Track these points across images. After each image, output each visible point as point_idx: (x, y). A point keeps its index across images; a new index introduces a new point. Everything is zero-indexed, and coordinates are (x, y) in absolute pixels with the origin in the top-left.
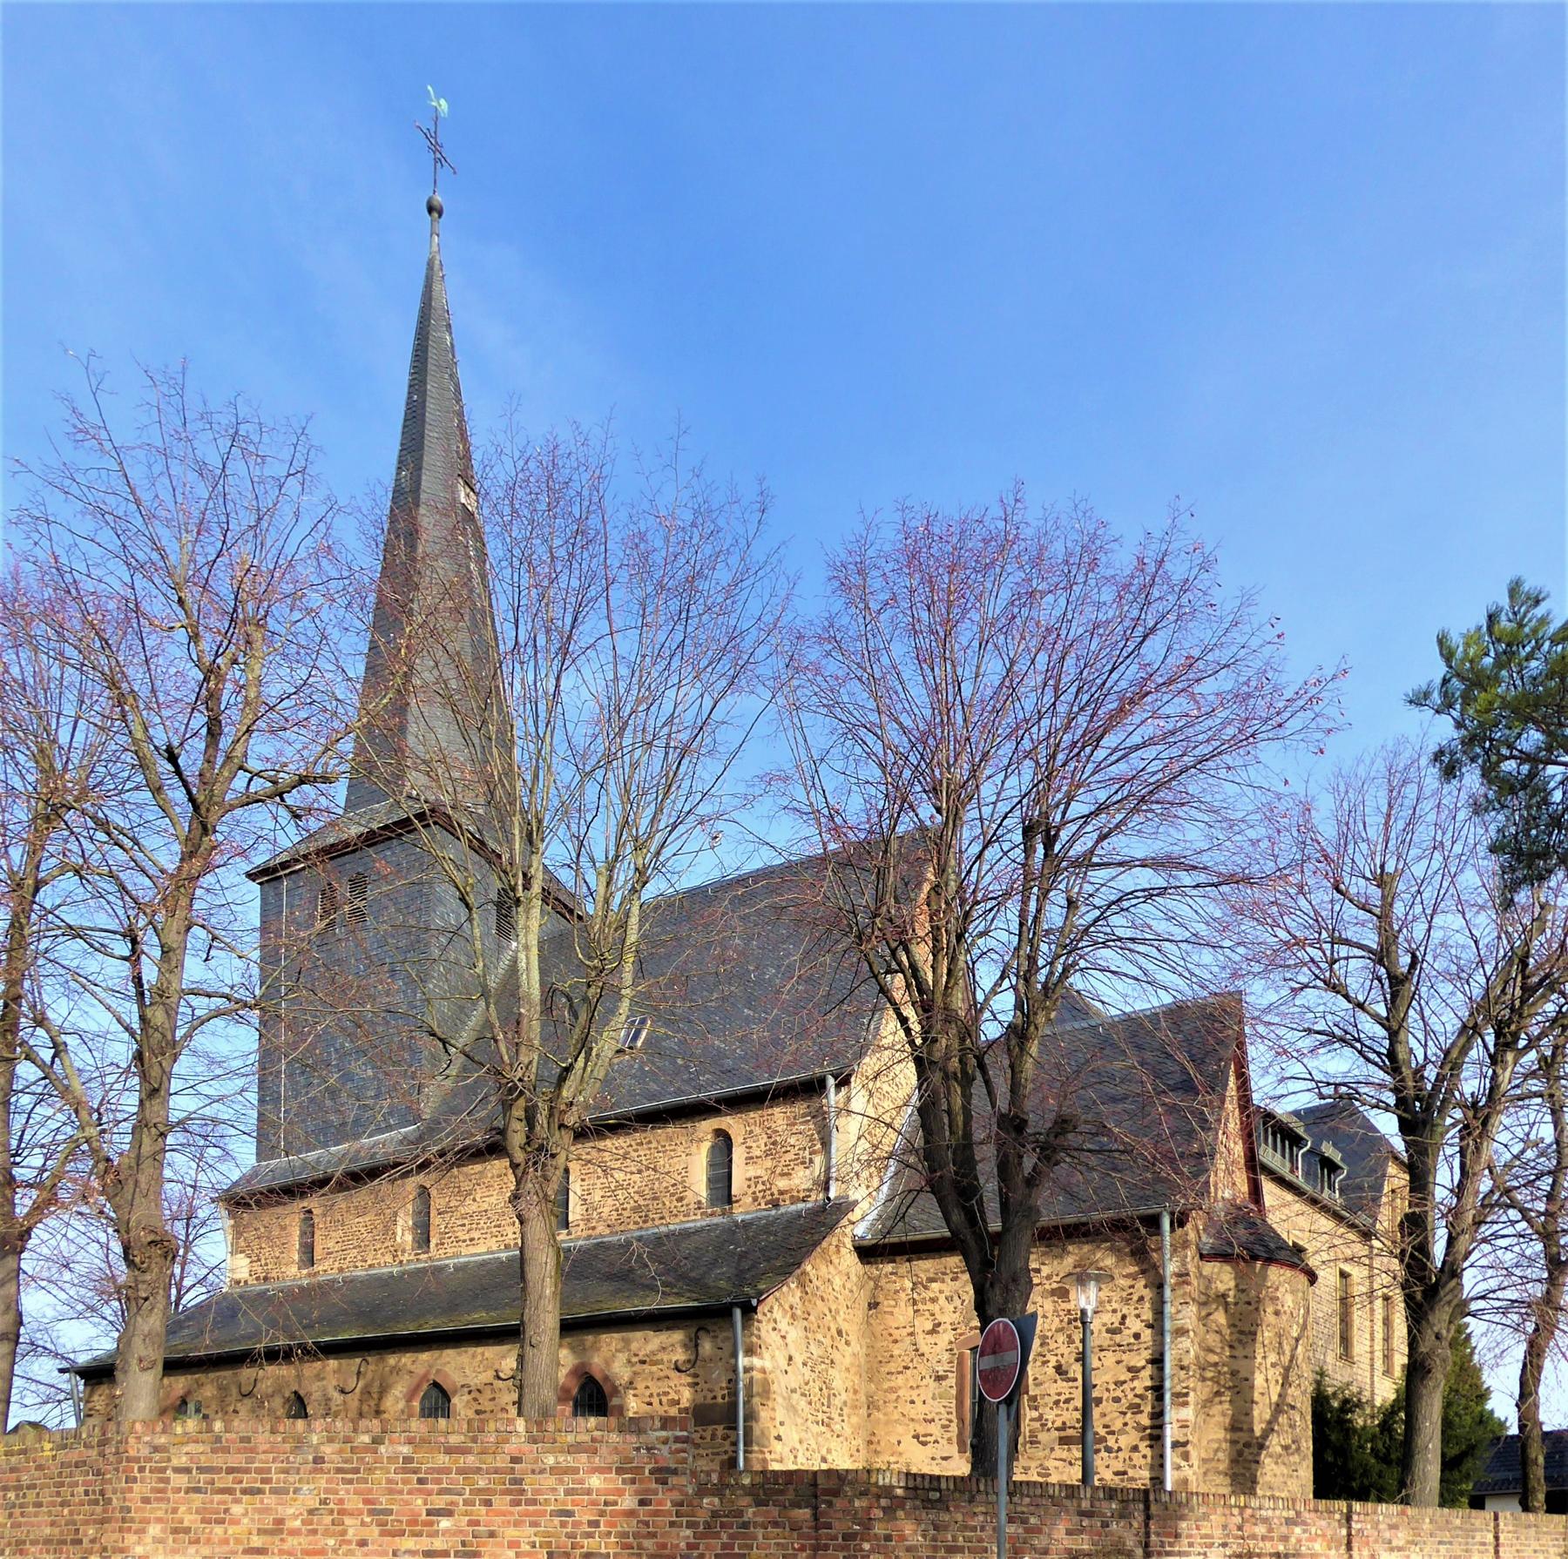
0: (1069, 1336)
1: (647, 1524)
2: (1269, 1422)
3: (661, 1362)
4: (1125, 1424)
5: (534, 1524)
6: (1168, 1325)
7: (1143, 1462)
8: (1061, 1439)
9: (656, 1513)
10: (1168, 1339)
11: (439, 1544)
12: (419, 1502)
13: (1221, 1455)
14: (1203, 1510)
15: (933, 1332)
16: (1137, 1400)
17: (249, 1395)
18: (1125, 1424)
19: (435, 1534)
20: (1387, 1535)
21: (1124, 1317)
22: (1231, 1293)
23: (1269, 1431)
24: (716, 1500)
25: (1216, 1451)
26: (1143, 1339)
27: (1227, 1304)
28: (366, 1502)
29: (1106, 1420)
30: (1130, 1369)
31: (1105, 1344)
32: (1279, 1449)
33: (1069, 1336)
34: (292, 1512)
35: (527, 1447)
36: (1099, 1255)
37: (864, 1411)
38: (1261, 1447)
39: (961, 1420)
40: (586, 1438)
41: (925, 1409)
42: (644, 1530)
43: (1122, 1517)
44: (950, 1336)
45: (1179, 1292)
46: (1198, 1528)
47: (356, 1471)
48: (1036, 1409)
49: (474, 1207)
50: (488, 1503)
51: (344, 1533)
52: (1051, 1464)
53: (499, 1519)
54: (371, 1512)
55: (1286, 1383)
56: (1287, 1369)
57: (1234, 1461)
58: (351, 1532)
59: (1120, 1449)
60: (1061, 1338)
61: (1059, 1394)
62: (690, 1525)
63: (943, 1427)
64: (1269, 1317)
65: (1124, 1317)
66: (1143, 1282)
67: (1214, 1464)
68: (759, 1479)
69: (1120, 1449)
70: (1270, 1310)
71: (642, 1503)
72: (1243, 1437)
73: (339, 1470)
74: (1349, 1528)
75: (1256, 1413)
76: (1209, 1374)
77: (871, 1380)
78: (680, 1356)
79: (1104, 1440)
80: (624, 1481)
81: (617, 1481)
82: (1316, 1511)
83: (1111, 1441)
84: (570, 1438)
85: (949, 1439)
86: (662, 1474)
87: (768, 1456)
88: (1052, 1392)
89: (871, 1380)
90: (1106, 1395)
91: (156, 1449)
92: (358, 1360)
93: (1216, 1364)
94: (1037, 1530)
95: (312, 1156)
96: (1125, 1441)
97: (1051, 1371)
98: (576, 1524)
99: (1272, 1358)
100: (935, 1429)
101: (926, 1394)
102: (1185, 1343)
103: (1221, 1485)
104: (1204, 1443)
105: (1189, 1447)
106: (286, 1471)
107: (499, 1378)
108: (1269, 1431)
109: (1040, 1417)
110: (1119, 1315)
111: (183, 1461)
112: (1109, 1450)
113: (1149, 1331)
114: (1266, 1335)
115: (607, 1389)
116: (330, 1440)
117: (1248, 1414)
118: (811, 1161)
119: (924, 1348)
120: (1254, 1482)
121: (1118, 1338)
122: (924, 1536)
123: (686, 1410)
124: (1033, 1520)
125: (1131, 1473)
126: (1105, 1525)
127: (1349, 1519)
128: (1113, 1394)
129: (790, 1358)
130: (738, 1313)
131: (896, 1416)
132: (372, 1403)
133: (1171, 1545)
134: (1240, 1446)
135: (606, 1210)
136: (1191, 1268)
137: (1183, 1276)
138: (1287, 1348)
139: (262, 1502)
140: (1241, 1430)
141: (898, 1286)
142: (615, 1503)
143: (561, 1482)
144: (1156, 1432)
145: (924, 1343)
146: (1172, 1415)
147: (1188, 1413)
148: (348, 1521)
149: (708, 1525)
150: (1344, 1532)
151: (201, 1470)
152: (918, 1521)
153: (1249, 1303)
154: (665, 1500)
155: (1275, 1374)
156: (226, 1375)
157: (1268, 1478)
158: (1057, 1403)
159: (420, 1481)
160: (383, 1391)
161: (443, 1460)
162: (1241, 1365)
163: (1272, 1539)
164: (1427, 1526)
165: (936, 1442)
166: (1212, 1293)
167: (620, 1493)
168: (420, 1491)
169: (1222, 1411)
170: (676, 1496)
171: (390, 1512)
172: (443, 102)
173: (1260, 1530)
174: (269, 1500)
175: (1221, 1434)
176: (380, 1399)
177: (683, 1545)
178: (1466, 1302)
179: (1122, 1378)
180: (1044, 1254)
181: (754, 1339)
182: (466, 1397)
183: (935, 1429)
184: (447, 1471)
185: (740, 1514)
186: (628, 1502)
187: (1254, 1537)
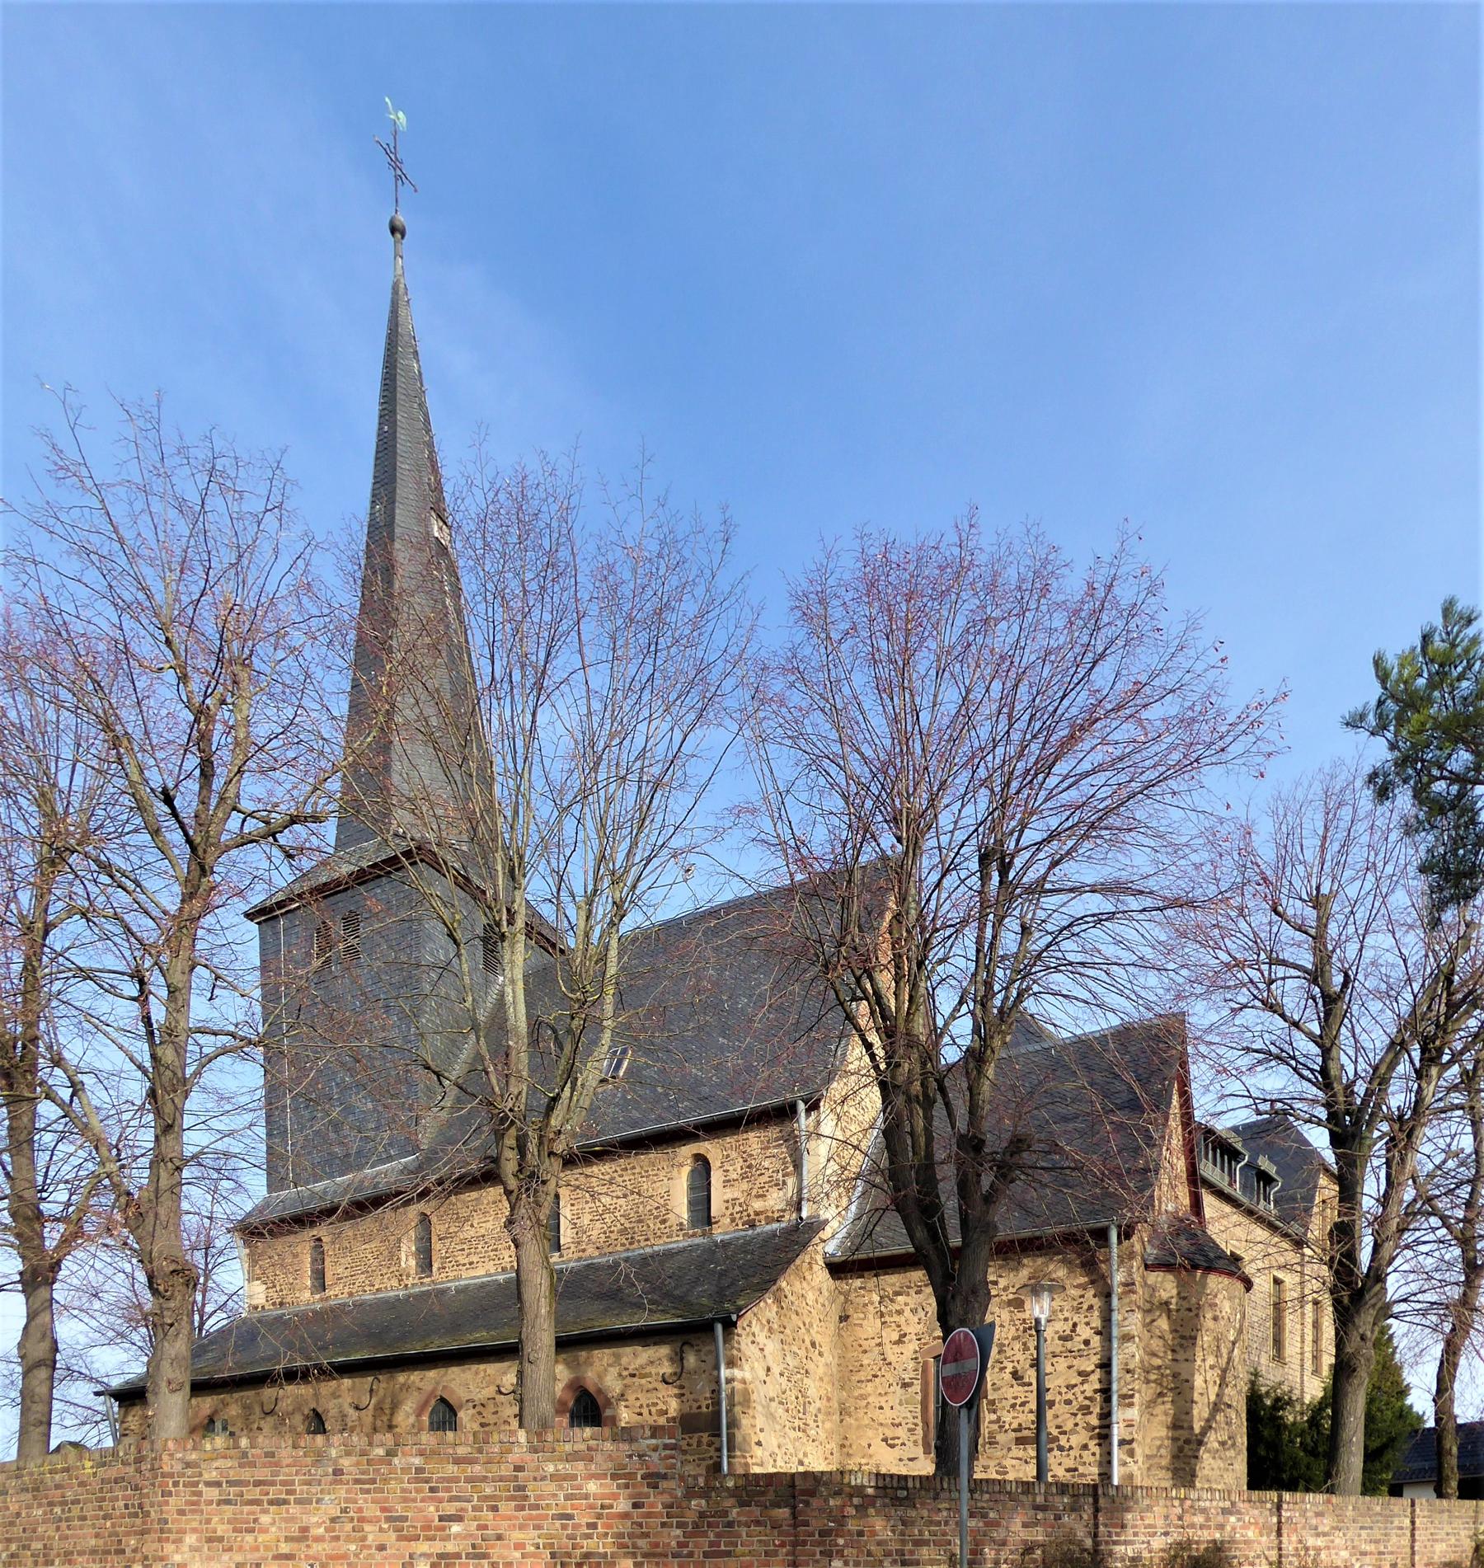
0: (1024, 1344)
1: (640, 1525)
2: (1208, 1420)
3: (649, 1375)
4: (1076, 1425)
5: (537, 1527)
6: (1115, 1332)
7: (1092, 1459)
8: (1017, 1439)
9: (649, 1515)
10: (1115, 1345)
11: (451, 1547)
12: (432, 1509)
13: (1163, 1451)
14: (1147, 1502)
15: (899, 1342)
16: (1087, 1402)
17: (271, 1413)
18: (1076, 1425)
19: (447, 1538)
20: (1314, 1522)
21: (1075, 1325)
22: (1174, 1301)
23: (1207, 1428)
24: (703, 1502)
25: (1159, 1448)
26: (1092, 1345)
27: (1169, 1311)
28: (383, 1510)
29: (1059, 1421)
30: (1080, 1374)
31: (1058, 1351)
32: (1216, 1445)
33: (1024, 1344)
34: (316, 1521)
35: (528, 1457)
36: (1051, 1267)
37: (836, 1417)
38: (1200, 1443)
39: (926, 1423)
40: (582, 1447)
41: (893, 1414)
42: (638, 1531)
43: (1073, 1510)
44: (914, 1346)
45: (1126, 1300)
46: (1142, 1519)
47: (373, 1481)
48: (994, 1412)
49: (472, 1233)
50: (495, 1509)
51: (364, 1539)
52: (1008, 1462)
53: (505, 1523)
54: (388, 1519)
55: (1223, 1383)
56: (1224, 1371)
57: (1175, 1457)
58: (370, 1537)
59: (1071, 1448)
60: (1017, 1346)
61: (1015, 1398)
62: (680, 1525)
63: (910, 1430)
64: (1209, 1323)
65: (1075, 1325)
66: (1092, 1292)
67: (1156, 1460)
68: (741, 1482)
69: (1071, 1448)
70: (1209, 1315)
71: (635, 1506)
72: (1184, 1434)
73: (357, 1481)
74: (1280, 1516)
75: (1195, 1412)
76: (1153, 1377)
77: (842, 1388)
78: (667, 1369)
79: (1056, 1439)
80: (618, 1487)
81: (612, 1486)
82: (1250, 1501)
83: (1063, 1441)
84: (568, 1447)
85: (915, 1442)
86: (654, 1479)
87: (749, 1460)
88: (1009, 1396)
89: (842, 1388)
90: (1058, 1398)
91: (188, 1465)
92: (370, 1379)
93: (1159, 1367)
94: (996, 1524)
95: (319, 1186)
96: (1076, 1441)
97: (1007, 1376)
98: (576, 1527)
99: (1211, 1360)
100: (901, 1432)
101: (893, 1400)
102: (1131, 1348)
103: (1163, 1479)
104: (1148, 1440)
105: (1135, 1445)
106: (308, 1483)
107: (501, 1393)
108: (1207, 1428)
109: (999, 1419)
110: (1071, 1323)
111: (213, 1475)
112: (1061, 1448)
113: (1098, 1338)
114: (1205, 1339)
115: (600, 1401)
116: (348, 1454)
117: (1188, 1413)
118: (784, 1183)
119: (891, 1358)
120: (1194, 1475)
121: (1069, 1344)
122: (893, 1531)
123: (674, 1419)
124: (992, 1515)
125: (1081, 1469)
126: (1058, 1518)
127: (1279, 1508)
128: (1065, 1397)
129: (768, 1369)
130: (719, 1327)
131: (866, 1421)
132: (385, 1419)
133: (1118, 1534)
134: (1180, 1443)
135: (595, 1233)
136: (1137, 1278)
137: (1129, 1285)
138: (1224, 1351)
139: (287, 1511)
140: (1182, 1428)
141: (866, 1300)
142: (611, 1507)
143: (561, 1488)
144: (1104, 1431)
145: (891, 1353)
146: (1119, 1415)
147: (1133, 1413)
148: (367, 1527)
149: (696, 1525)
150: (1275, 1520)
151: (230, 1483)
152: (888, 1517)
153: (1190, 1310)
154: (656, 1503)
155: (1213, 1376)
156: (249, 1394)
157: (1206, 1472)
158: (1013, 1406)
159: (432, 1490)
160: (395, 1407)
161: (452, 1469)
162: (1182, 1367)
163: (1209, 1527)
164: (1350, 1513)
165: (903, 1444)
166: (1156, 1301)
167: (615, 1497)
168: (432, 1499)
169: (1165, 1411)
170: (667, 1499)
171: (406, 1519)
172: (401, 114)
173: (1199, 1519)
174: (294, 1509)
175: (1164, 1432)
176: (392, 1414)
177: (674, 1544)
178: (1389, 1305)
179: (1073, 1382)
180: (1001, 1267)
181: (735, 1352)
182: (471, 1411)
183: (901, 1432)
184: (456, 1480)
185: (725, 1513)
186: (622, 1505)
187: (1192, 1526)
